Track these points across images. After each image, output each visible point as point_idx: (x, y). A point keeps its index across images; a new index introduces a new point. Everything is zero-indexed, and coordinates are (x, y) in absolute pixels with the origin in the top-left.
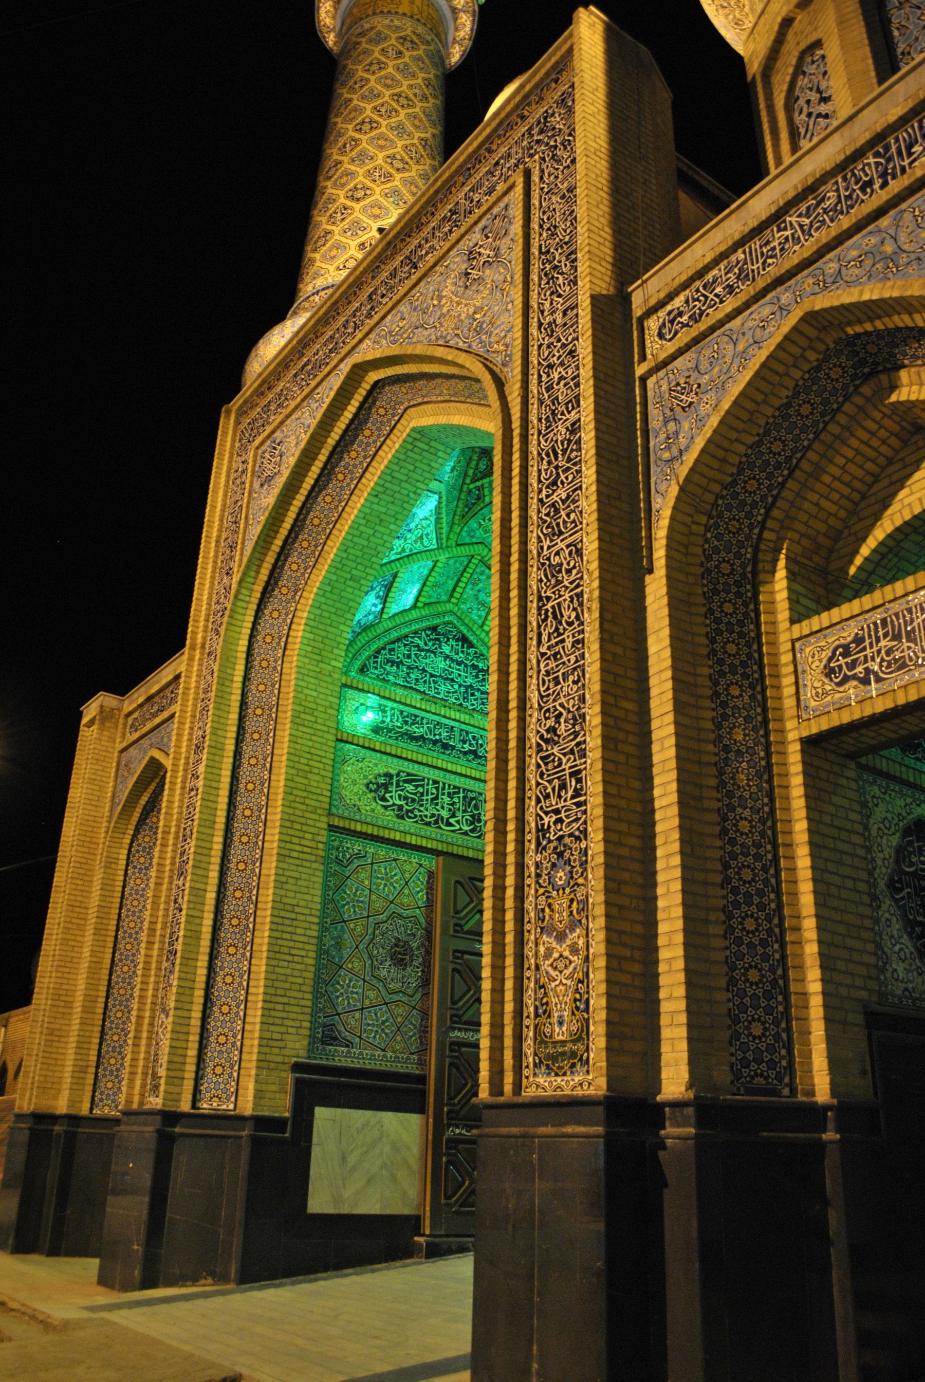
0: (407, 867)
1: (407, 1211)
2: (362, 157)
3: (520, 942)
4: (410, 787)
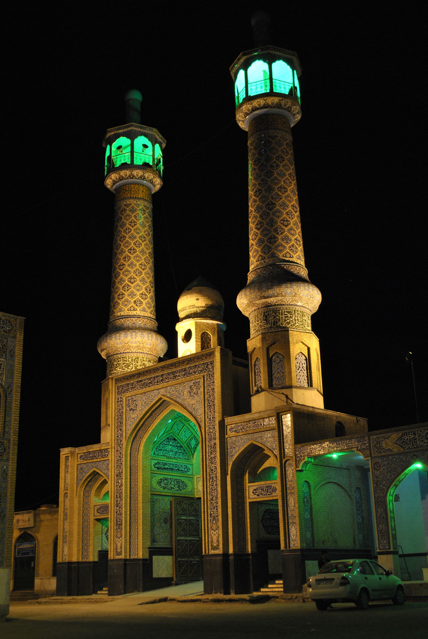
0: (166, 500)
1: (170, 576)
2: (132, 265)
3: (208, 531)
4: (166, 481)
